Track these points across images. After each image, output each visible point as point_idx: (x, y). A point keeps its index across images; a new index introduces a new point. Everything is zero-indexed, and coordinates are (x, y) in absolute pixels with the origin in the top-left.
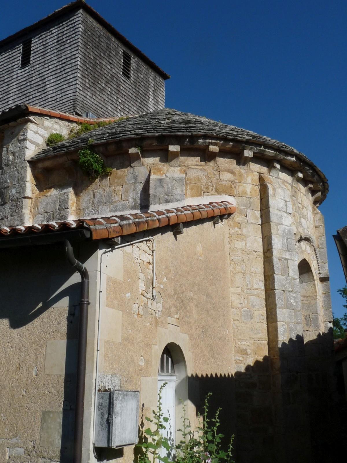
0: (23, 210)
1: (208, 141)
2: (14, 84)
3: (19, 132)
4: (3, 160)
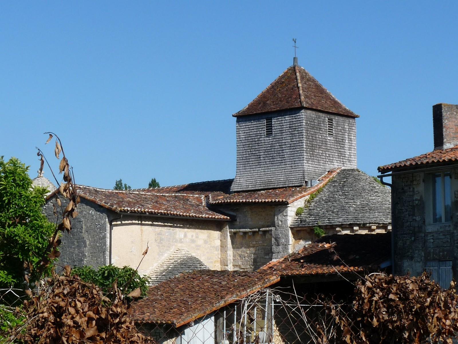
0: (289, 251)
1: (371, 225)
2: (263, 146)
3: (284, 210)
4: (276, 223)
